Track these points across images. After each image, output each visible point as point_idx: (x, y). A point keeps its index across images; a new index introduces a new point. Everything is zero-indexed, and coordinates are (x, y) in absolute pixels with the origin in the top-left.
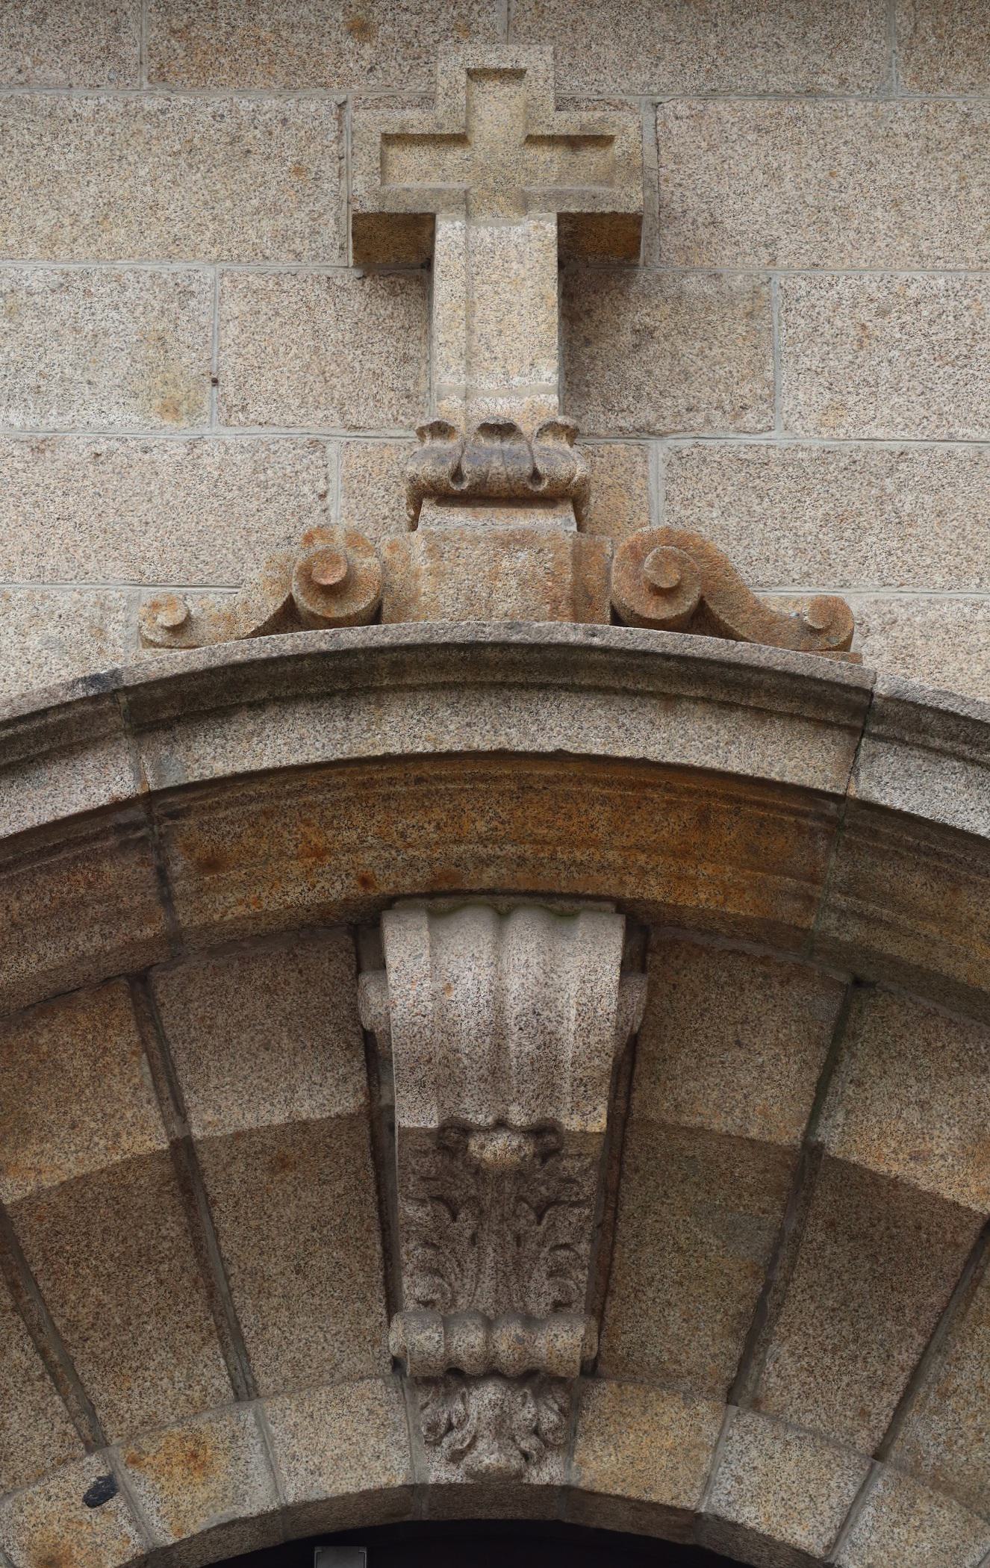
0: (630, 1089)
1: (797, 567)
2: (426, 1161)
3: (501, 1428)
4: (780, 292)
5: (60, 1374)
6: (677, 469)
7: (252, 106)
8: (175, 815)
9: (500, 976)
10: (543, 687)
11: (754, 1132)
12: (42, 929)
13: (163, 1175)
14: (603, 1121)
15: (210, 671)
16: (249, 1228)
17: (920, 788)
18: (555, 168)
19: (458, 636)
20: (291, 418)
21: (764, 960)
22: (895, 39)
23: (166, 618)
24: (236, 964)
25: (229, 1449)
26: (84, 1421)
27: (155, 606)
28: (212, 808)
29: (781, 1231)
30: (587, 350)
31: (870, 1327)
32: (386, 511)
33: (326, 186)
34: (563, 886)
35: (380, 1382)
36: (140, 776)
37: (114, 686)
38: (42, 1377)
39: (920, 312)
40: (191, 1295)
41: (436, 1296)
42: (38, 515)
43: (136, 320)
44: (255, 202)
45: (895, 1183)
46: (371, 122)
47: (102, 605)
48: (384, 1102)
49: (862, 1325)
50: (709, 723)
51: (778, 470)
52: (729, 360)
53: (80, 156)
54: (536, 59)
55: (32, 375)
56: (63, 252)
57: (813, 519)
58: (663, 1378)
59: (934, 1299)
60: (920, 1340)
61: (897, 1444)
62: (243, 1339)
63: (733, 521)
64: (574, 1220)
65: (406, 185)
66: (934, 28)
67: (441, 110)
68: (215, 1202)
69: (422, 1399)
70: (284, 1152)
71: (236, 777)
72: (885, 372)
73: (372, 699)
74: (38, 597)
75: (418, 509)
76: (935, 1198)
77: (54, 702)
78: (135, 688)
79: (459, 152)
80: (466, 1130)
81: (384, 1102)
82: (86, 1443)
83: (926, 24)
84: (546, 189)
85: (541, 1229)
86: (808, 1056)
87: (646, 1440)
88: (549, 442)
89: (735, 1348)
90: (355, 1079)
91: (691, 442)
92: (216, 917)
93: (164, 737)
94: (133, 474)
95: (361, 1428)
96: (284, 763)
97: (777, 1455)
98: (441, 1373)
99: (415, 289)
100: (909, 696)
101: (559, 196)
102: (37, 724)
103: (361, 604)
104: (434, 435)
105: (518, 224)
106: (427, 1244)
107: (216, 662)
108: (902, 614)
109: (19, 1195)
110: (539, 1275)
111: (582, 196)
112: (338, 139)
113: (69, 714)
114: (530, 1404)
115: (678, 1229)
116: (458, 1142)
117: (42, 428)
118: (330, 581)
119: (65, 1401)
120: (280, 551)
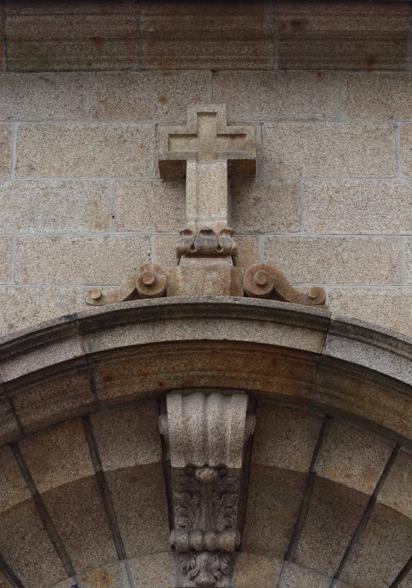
0: (251, 454)
1: (308, 277)
2: (182, 478)
3: (208, 568)
4: (303, 185)
5: (60, 551)
6: (268, 245)
7: (127, 126)
8: (96, 362)
9: (205, 415)
10: (219, 318)
11: (292, 468)
12: (52, 400)
13: (93, 483)
14: (241, 465)
15: (107, 314)
16: (123, 501)
17: (346, 351)
18: (227, 145)
19: (191, 300)
20: (139, 229)
21: (296, 410)
22: (341, 102)
23: (94, 296)
24: (118, 412)
25: (116, 576)
26: (68, 566)
27: (90, 292)
28: (109, 360)
29: (303, 502)
30: (238, 205)
31: (333, 534)
32: (170, 260)
33: (151, 152)
34: (228, 385)
35: (167, 553)
36: (83, 349)
37: (75, 319)
38: (54, 552)
39: (350, 192)
40: (104, 524)
41: (186, 524)
42: (54, 262)
43: (87, 197)
44: (127, 157)
45: (340, 485)
46: (165, 130)
47: (75, 292)
48: (168, 459)
49: (330, 533)
50: (275, 330)
51: (302, 245)
52: (286, 208)
53: (69, 143)
54: (220, 109)
55: (53, 216)
56: (63, 175)
57: (314, 261)
58: (263, 552)
59: (354, 524)
60: (350, 538)
61: (342, 573)
62: (121, 539)
63: (287, 262)
64: (232, 498)
65: (177, 151)
66: (354, 98)
67: (189, 126)
68: (111, 493)
69: (181, 559)
70: (135, 475)
71: (116, 349)
72: (338, 212)
73: (162, 322)
74: (53, 289)
75: (180, 259)
76: (353, 490)
77: (55, 324)
78: (82, 319)
79: (194, 140)
80: (195, 468)
81: (168, 459)
82: (69, 574)
83: (352, 97)
84: (223, 152)
85: (221, 501)
86: (311, 442)
87: (257, 572)
88: (224, 236)
89: (287, 541)
90: (158, 451)
91: (273, 236)
92: (111, 396)
93: (92, 336)
94: (86, 248)
95: (161, 569)
96: (132, 344)
97: (301, 577)
98: (187, 550)
99: (180, 185)
100: (342, 320)
101: (228, 154)
102: (49, 331)
103: (159, 291)
104: (185, 234)
105: (214, 163)
106: (183, 506)
107: (109, 310)
108: (344, 293)
109: (45, 490)
110: (221, 517)
111: (235, 154)
112: (155, 136)
113: (60, 328)
114: (217, 560)
115: (268, 501)
116: (192, 472)
117: (56, 233)
118: (149, 283)
119: (61, 560)
120: (132, 273)
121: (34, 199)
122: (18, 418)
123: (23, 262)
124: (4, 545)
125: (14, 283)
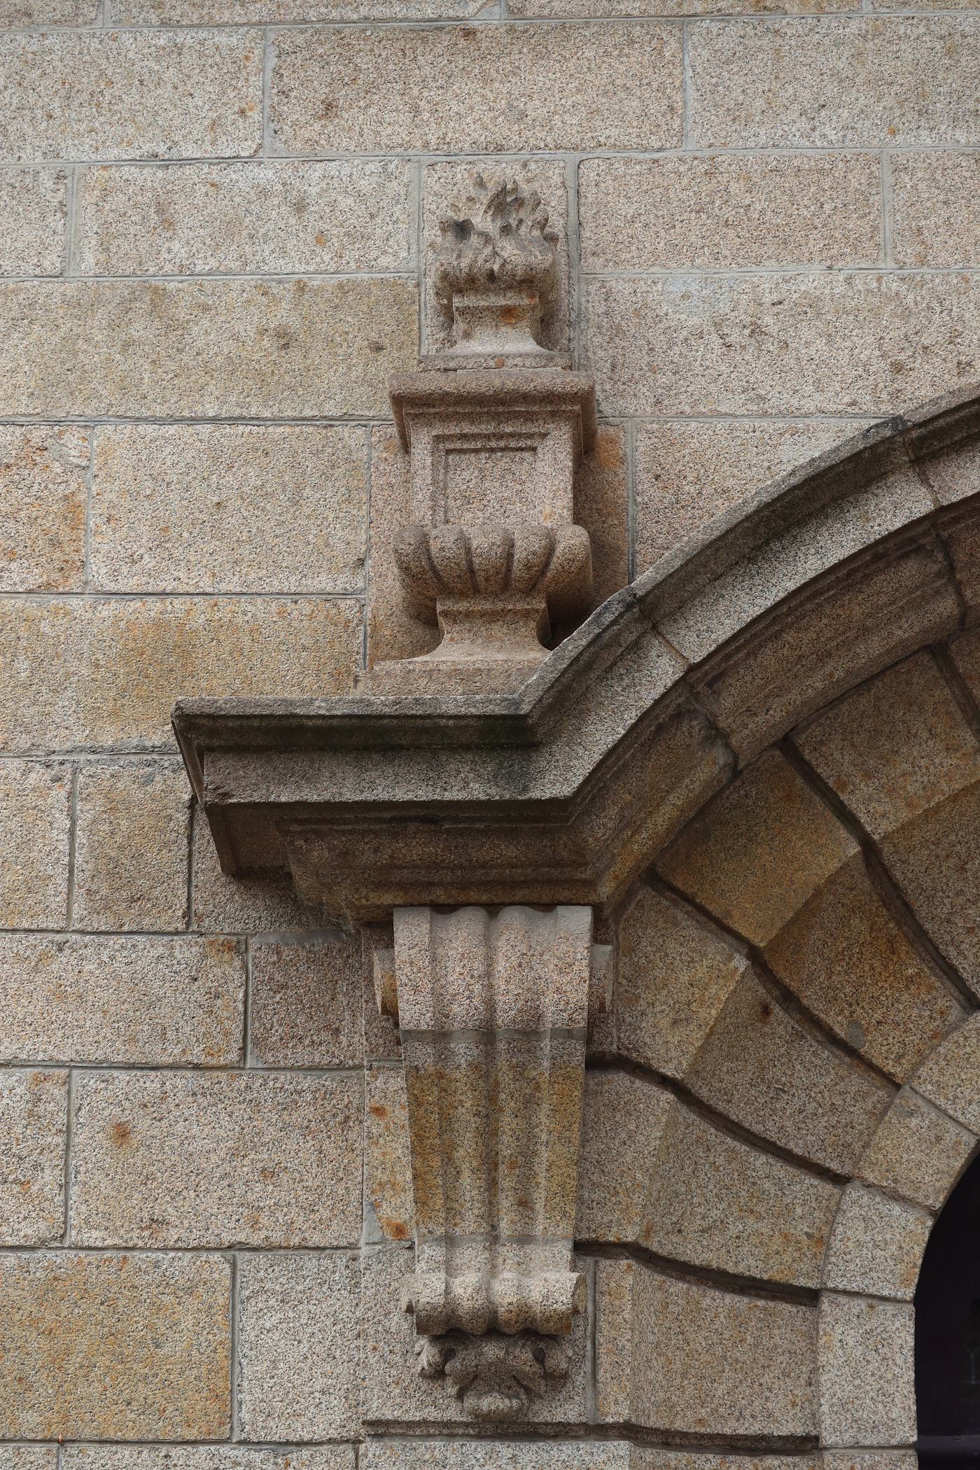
121: (922, 61)
122: (959, 588)
123: (912, 213)
124: (919, 886)
125: (895, 266)
